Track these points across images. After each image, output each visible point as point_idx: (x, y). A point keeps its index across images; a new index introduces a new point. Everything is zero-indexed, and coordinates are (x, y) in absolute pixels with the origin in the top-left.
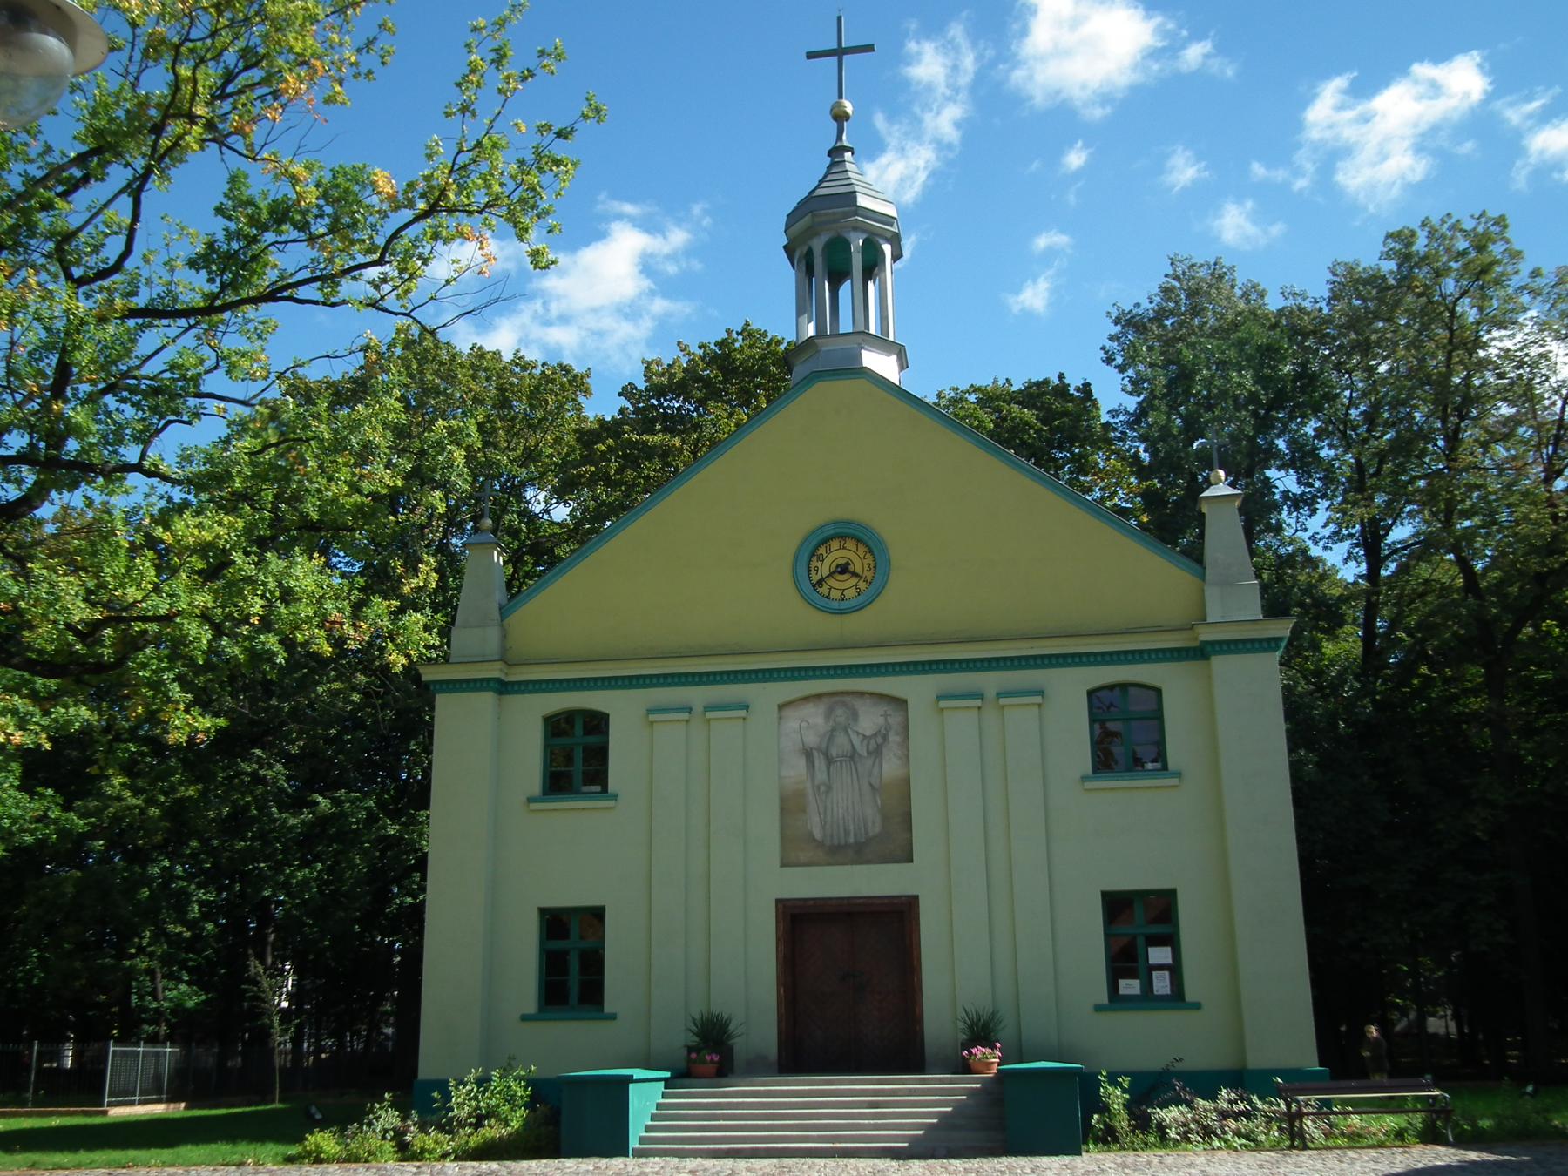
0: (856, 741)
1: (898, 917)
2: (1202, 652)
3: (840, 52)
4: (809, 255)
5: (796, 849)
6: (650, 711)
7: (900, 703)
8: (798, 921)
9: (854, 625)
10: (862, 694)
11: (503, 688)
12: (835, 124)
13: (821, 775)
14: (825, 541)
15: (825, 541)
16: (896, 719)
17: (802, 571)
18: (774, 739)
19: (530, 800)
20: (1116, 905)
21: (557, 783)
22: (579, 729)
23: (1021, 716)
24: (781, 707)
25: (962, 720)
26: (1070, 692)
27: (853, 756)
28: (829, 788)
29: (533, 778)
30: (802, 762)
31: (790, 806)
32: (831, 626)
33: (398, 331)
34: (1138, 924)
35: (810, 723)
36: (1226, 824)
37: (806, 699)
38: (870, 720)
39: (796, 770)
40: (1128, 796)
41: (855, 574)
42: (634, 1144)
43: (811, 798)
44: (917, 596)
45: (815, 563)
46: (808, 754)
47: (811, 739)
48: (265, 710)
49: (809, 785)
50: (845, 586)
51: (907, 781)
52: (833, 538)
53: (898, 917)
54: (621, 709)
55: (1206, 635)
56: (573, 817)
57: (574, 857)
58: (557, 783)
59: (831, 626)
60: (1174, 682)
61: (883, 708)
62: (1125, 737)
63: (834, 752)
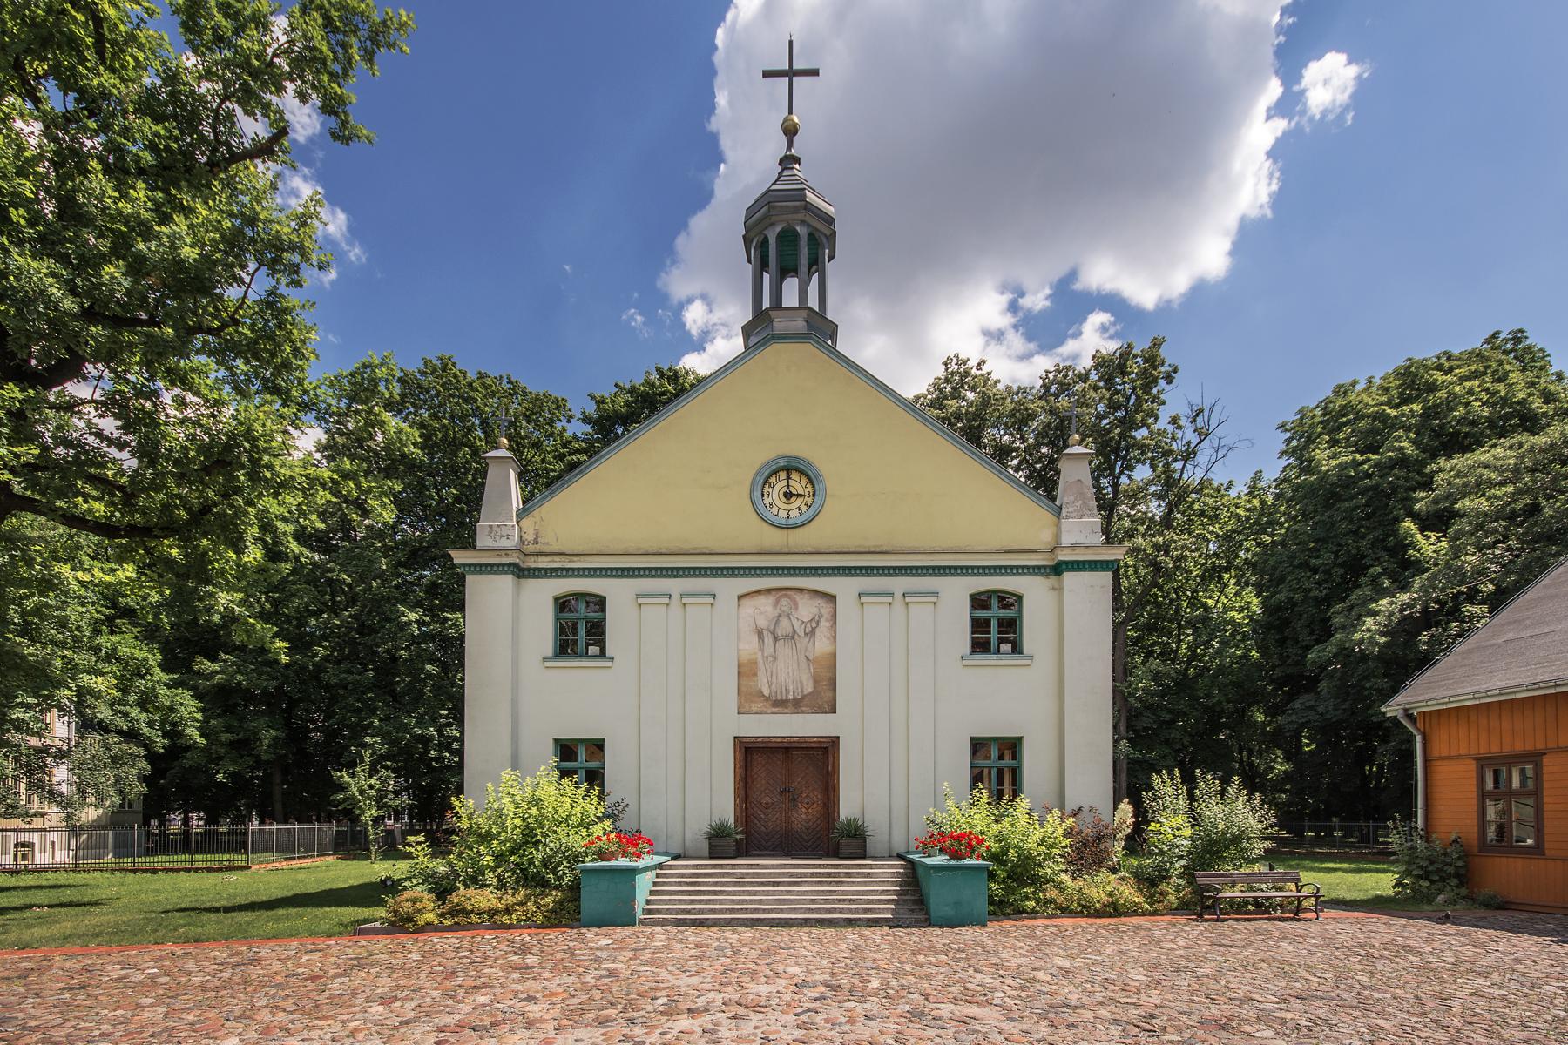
0: (796, 624)
1: (823, 754)
2: (1058, 569)
3: (791, 73)
4: (764, 244)
5: (748, 698)
6: (638, 596)
7: (831, 598)
8: (750, 753)
9: (796, 538)
10: (801, 590)
11: (521, 573)
12: (784, 140)
13: (769, 650)
14: (775, 472)
15: (775, 472)
16: (826, 609)
17: (757, 494)
18: (729, 622)
19: (545, 659)
20: (978, 746)
21: (565, 648)
22: (995, 603)
23: (921, 612)
24: (740, 597)
25: (876, 613)
26: (957, 591)
27: (793, 636)
28: (775, 659)
29: (548, 644)
30: (755, 639)
31: (746, 671)
32: (775, 538)
33: (365, 366)
34: (997, 765)
35: (764, 608)
36: (1065, 690)
37: (759, 592)
38: (807, 609)
39: (750, 646)
40: (997, 672)
41: (799, 495)
42: (639, 915)
43: (761, 664)
44: (842, 521)
45: (767, 489)
46: (760, 634)
47: (763, 623)
48: (1040, 460)
49: (759, 656)
50: (795, 508)
51: (834, 655)
52: (770, 476)
53: (823, 754)
54: (617, 593)
55: (1064, 556)
56: (579, 674)
57: (576, 698)
58: (565, 648)
59: (775, 538)
60: (1034, 591)
61: (819, 601)
62: (995, 628)
63: (779, 632)
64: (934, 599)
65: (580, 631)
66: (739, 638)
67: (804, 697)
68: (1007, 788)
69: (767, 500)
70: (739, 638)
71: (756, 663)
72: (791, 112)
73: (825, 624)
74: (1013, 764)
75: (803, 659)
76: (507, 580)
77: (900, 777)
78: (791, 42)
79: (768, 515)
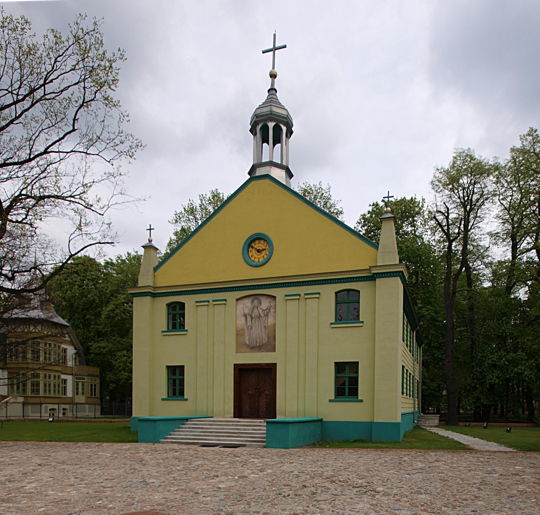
0: (260, 311)
2: (373, 278)
5: (241, 346)
11: (154, 295)
13: (249, 323)
18: (234, 312)
20: (340, 367)
23: (312, 304)
26: (329, 292)
27: (259, 317)
28: (252, 327)
30: (244, 319)
31: (239, 334)
34: (347, 381)
38: (265, 303)
39: (241, 322)
41: (264, 250)
46: (245, 316)
47: (247, 311)
49: (245, 327)
51: (275, 324)
53: (269, 371)
54: (188, 301)
61: (269, 300)
62: (347, 309)
63: (253, 315)
64: (318, 296)
65: (176, 318)
66: (236, 319)
67: (263, 344)
68: (532, 465)
69: (250, 254)
70: (236, 319)
71: (243, 330)
72: (273, 68)
73: (272, 310)
74: (181, 377)
75: (263, 327)
76: (148, 298)
77: (302, 393)
78: (275, 35)
79: (251, 263)
